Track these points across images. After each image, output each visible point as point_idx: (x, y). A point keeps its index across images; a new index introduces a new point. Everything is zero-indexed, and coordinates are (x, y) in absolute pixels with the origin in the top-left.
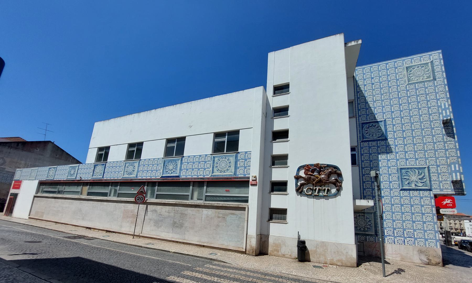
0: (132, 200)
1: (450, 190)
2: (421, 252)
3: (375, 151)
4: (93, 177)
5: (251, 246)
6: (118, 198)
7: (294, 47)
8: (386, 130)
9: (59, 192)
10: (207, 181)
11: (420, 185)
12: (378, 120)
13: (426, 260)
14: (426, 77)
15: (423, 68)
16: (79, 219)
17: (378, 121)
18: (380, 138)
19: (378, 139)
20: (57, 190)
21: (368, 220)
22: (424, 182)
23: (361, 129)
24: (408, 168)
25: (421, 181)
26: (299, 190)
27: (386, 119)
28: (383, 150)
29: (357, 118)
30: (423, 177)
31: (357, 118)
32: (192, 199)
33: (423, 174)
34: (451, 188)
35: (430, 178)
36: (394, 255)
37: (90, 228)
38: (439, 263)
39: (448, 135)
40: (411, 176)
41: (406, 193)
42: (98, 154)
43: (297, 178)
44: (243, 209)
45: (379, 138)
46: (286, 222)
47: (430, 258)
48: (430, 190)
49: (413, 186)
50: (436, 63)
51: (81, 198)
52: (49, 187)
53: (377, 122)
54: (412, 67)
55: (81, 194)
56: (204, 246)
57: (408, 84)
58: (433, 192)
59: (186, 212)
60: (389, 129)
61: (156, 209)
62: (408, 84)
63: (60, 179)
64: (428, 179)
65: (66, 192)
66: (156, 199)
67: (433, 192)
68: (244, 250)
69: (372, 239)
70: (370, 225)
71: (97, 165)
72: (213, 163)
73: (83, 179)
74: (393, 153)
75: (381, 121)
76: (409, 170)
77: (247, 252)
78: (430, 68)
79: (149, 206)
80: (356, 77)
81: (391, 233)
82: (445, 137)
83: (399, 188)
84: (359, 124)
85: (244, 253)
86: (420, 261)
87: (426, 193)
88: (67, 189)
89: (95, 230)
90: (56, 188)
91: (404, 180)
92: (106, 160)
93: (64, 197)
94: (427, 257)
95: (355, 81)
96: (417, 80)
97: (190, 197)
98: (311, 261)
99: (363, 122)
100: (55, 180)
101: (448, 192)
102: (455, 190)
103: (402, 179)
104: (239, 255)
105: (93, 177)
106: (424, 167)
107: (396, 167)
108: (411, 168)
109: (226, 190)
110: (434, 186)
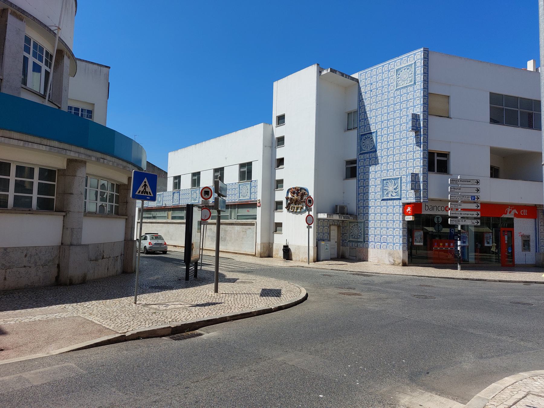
0: (139, 225)
1: (413, 199)
2: (390, 254)
3: (368, 163)
4: (173, 203)
5: (258, 251)
6: (212, 221)
7: (289, 76)
8: (376, 141)
9: (154, 217)
10: (238, 204)
11: (394, 194)
12: (372, 131)
13: (392, 261)
14: (409, 81)
15: (408, 70)
16: (169, 239)
17: (371, 132)
18: (372, 150)
19: (370, 151)
20: (152, 216)
21: (360, 228)
22: (397, 192)
23: (360, 141)
24: (388, 179)
25: (395, 191)
26: (288, 207)
27: (377, 129)
28: (373, 162)
29: (358, 130)
30: (397, 187)
31: (358, 130)
32: (231, 218)
33: (397, 185)
34: (414, 196)
35: (401, 188)
36: (374, 258)
37: (176, 246)
38: (400, 264)
39: (417, 144)
40: (389, 187)
41: (384, 203)
42: (175, 183)
43: (287, 199)
44: (253, 224)
45: (371, 149)
46: (281, 233)
47: (395, 259)
48: (400, 199)
49: (390, 197)
50: (418, 64)
51: (168, 222)
52: (146, 213)
53: (371, 133)
54: (400, 69)
55: (168, 218)
56: (236, 253)
57: (396, 90)
58: (402, 201)
59: (227, 229)
60: (379, 140)
61: (211, 228)
62: (396, 90)
63: (152, 206)
64: (400, 189)
65: (158, 217)
66: (212, 219)
67: (402, 201)
68: (254, 254)
69: (361, 245)
70: (361, 233)
71: (175, 192)
72: (239, 190)
73: (167, 205)
74: (379, 165)
75: (374, 132)
76: (388, 181)
77: (256, 255)
78: (413, 70)
79: (207, 225)
80: (360, 83)
81: (373, 239)
82: (415, 146)
83: (381, 198)
84: (359, 136)
85: (255, 255)
86: (389, 262)
87: (397, 202)
88: (158, 214)
89: (179, 247)
90: (151, 214)
91: (384, 191)
92: (179, 188)
93: (157, 221)
94: (393, 258)
95: (359, 88)
96: (403, 85)
97: (229, 218)
98: (293, 260)
99: (362, 134)
100: (149, 207)
101: (411, 201)
102: (416, 199)
103: (383, 189)
104: (251, 257)
105: (173, 203)
106: (397, 178)
107: (380, 179)
108: (390, 179)
109: (248, 211)
110: (403, 195)
